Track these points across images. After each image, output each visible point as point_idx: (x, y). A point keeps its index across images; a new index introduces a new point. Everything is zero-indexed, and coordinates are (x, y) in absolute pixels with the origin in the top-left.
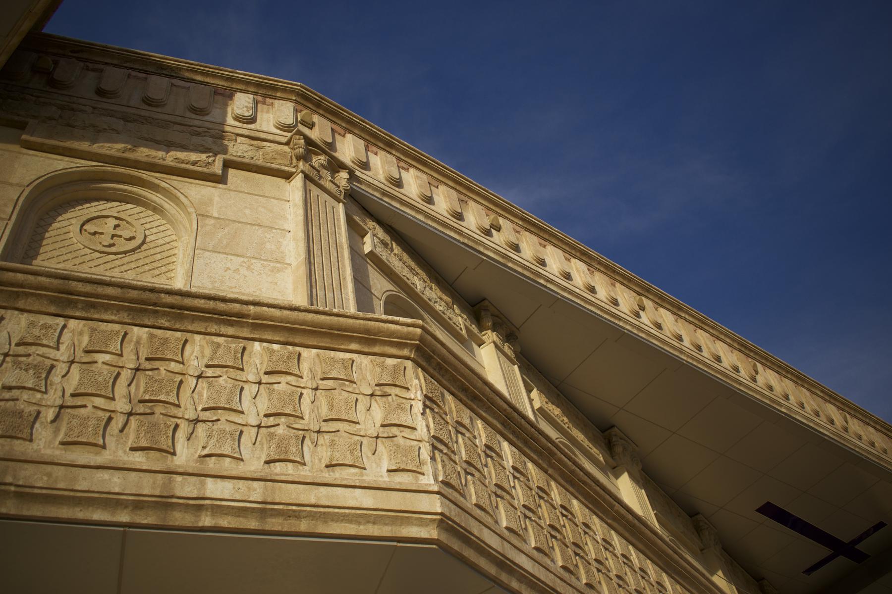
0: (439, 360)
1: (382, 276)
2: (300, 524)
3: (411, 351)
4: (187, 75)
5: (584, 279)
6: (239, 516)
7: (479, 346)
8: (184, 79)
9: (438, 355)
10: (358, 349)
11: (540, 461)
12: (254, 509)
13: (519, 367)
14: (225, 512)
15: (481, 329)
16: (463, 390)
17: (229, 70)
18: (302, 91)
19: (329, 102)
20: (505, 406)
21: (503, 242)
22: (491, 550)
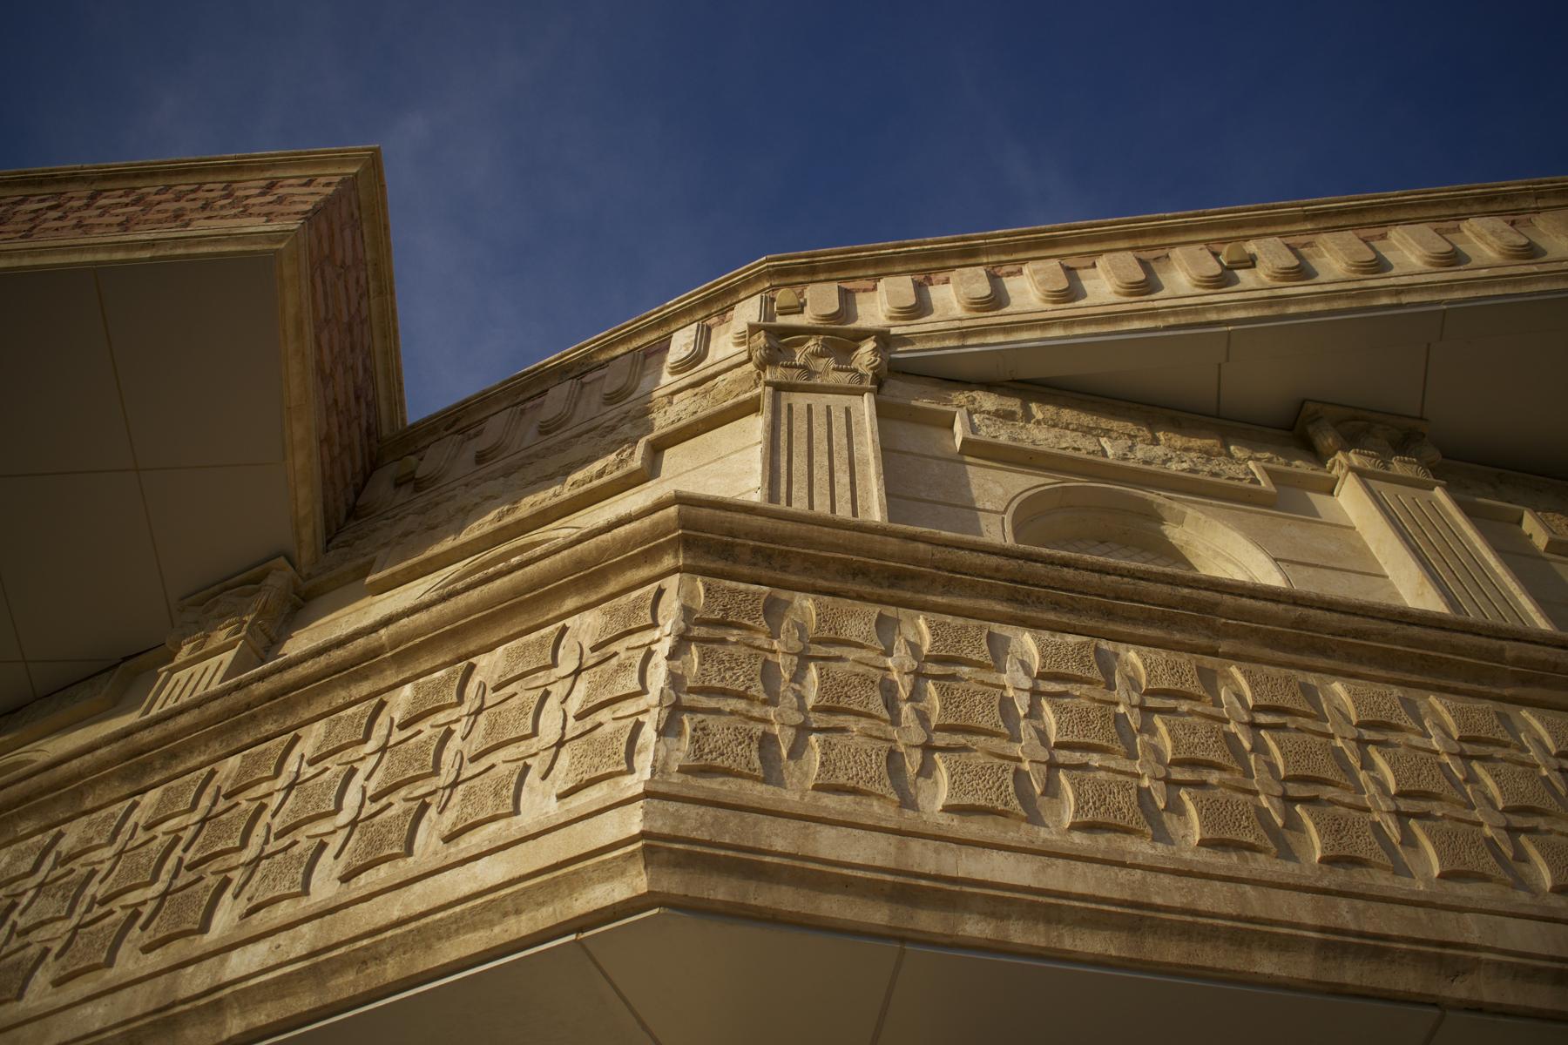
0: (751, 543)
1: (1028, 473)
2: (385, 969)
3: (676, 556)
4: (603, 357)
5: (1497, 243)
6: (283, 997)
7: (1331, 493)
8: (601, 366)
9: (747, 535)
10: (579, 604)
11: (1178, 636)
12: (298, 972)
13: (1448, 489)
14: (258, 998)
15: (1318, 457)
16: (855, 575)
17: (655, 310)
18: (773, 266)
19: (827, 254)
20: (994, 561)
21: (1267, 280)
22: (845, 871)
